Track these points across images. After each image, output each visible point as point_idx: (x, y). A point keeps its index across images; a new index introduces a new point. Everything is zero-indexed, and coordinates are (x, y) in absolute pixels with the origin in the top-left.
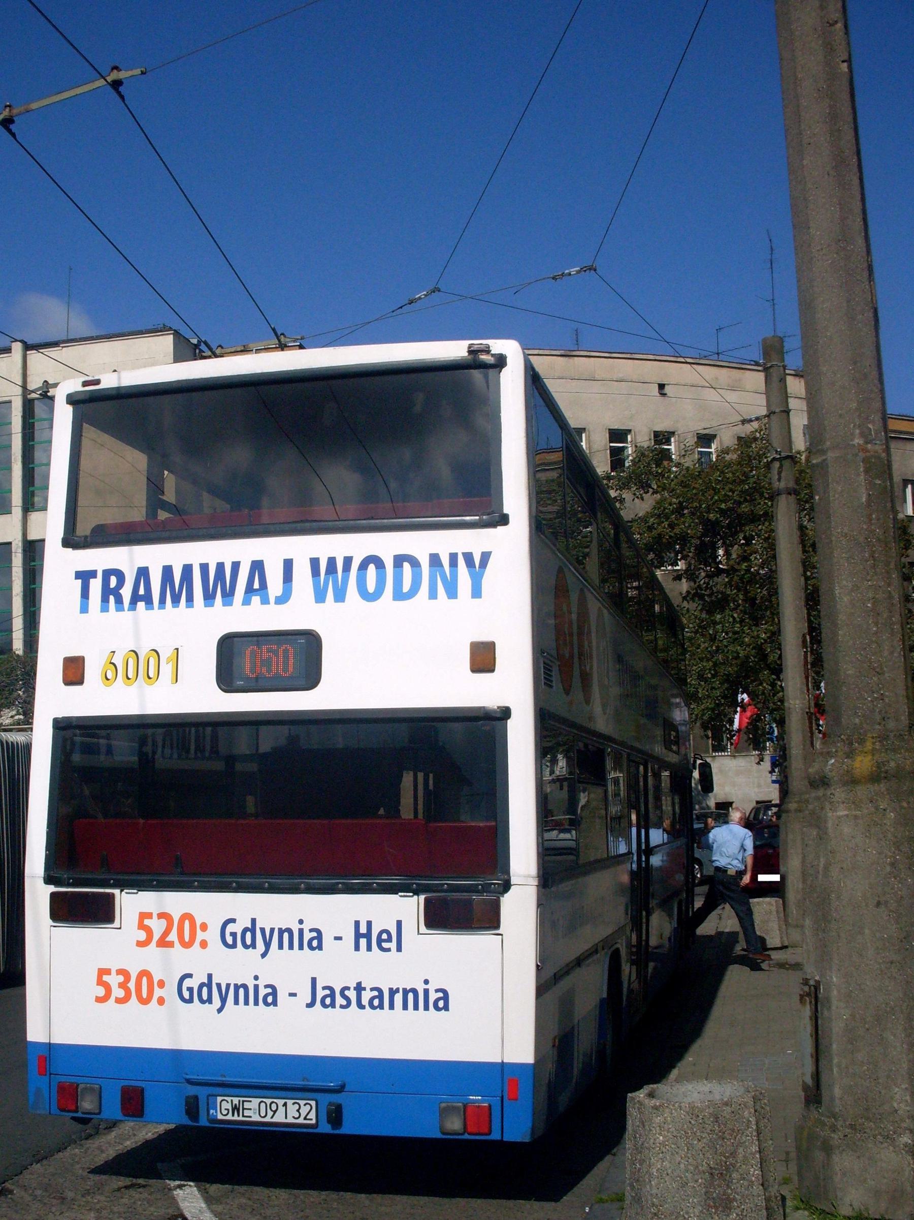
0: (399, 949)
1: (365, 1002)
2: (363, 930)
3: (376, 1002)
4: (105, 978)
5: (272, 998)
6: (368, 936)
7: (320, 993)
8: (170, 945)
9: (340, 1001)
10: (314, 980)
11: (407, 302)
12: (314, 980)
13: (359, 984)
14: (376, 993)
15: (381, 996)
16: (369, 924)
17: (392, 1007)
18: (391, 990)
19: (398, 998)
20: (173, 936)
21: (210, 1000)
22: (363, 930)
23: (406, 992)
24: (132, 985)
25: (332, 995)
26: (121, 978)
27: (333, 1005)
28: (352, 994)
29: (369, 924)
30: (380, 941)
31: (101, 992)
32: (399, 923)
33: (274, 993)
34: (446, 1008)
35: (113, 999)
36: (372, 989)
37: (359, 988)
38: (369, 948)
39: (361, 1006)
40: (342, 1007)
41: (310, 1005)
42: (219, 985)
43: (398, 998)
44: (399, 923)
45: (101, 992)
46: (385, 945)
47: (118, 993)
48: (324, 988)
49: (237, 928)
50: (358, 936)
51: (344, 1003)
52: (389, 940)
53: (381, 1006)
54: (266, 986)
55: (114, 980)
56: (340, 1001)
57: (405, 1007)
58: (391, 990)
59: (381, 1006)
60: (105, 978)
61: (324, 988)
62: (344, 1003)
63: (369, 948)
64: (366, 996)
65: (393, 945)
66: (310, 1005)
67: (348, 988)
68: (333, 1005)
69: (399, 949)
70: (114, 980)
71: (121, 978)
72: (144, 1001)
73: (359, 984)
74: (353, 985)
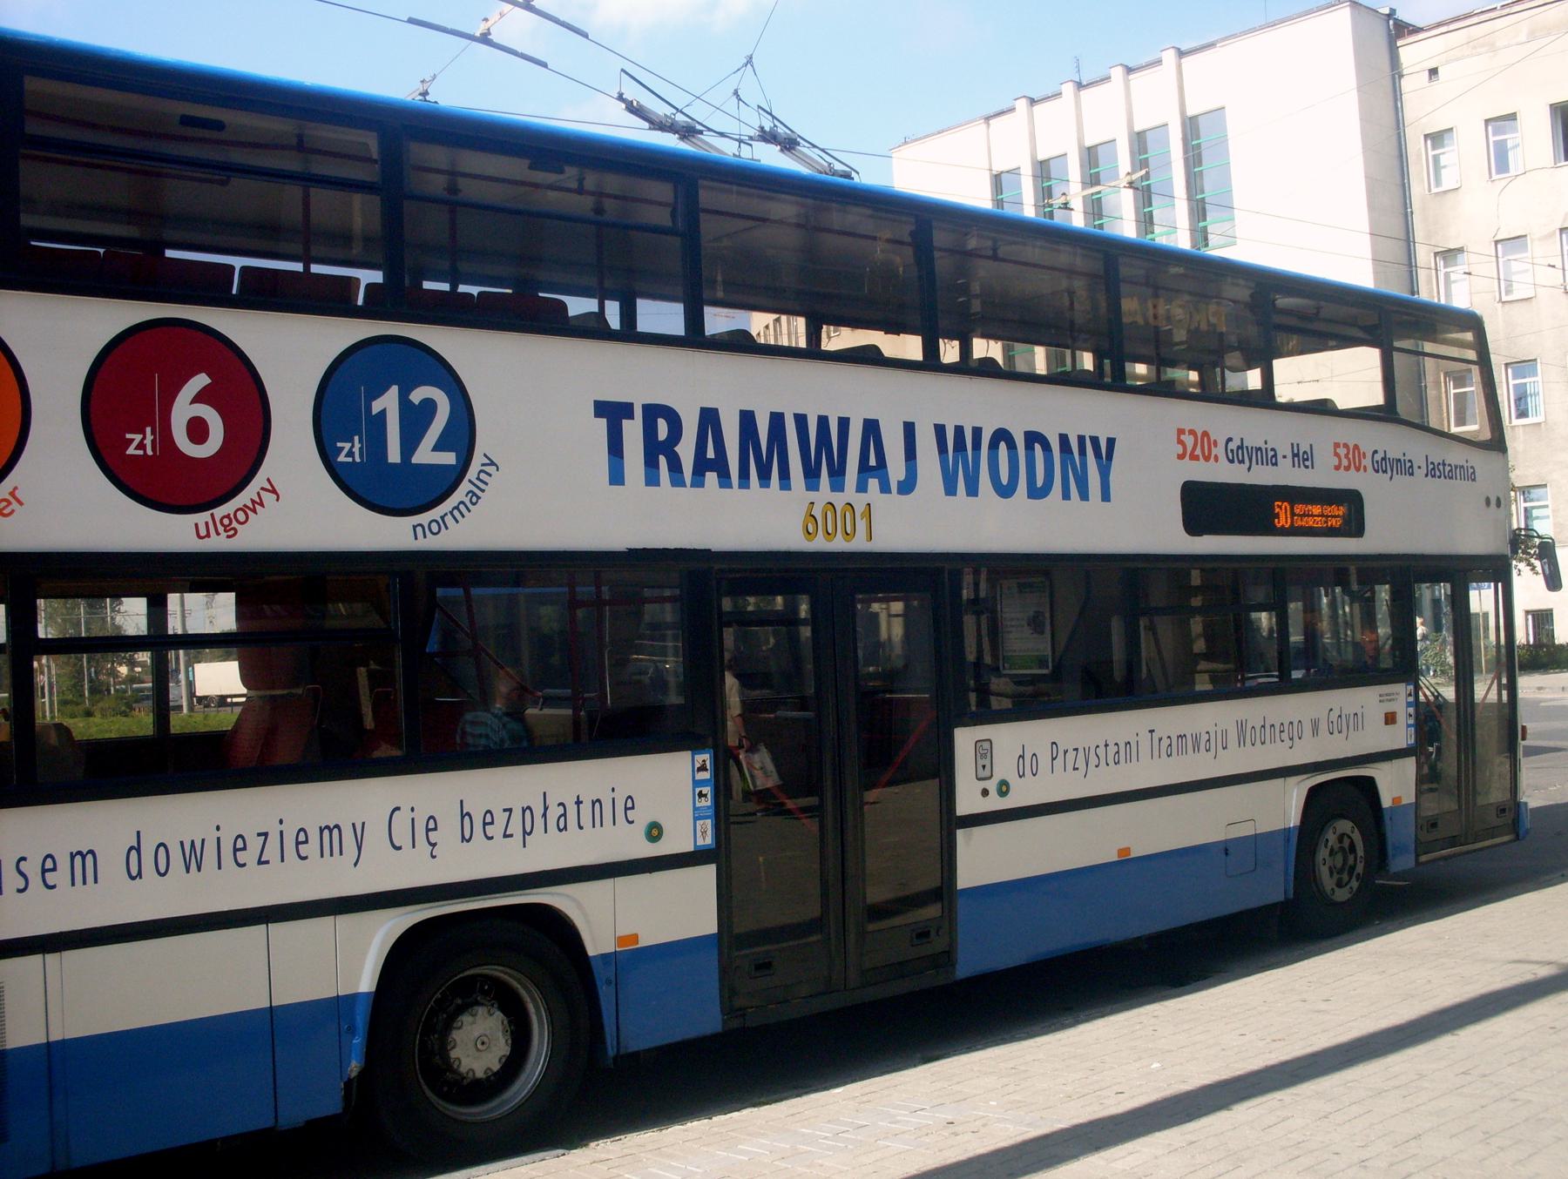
6: (1297, 455)
20: (1198, 452)
47: (1345, 462)
49: (1378, 457)
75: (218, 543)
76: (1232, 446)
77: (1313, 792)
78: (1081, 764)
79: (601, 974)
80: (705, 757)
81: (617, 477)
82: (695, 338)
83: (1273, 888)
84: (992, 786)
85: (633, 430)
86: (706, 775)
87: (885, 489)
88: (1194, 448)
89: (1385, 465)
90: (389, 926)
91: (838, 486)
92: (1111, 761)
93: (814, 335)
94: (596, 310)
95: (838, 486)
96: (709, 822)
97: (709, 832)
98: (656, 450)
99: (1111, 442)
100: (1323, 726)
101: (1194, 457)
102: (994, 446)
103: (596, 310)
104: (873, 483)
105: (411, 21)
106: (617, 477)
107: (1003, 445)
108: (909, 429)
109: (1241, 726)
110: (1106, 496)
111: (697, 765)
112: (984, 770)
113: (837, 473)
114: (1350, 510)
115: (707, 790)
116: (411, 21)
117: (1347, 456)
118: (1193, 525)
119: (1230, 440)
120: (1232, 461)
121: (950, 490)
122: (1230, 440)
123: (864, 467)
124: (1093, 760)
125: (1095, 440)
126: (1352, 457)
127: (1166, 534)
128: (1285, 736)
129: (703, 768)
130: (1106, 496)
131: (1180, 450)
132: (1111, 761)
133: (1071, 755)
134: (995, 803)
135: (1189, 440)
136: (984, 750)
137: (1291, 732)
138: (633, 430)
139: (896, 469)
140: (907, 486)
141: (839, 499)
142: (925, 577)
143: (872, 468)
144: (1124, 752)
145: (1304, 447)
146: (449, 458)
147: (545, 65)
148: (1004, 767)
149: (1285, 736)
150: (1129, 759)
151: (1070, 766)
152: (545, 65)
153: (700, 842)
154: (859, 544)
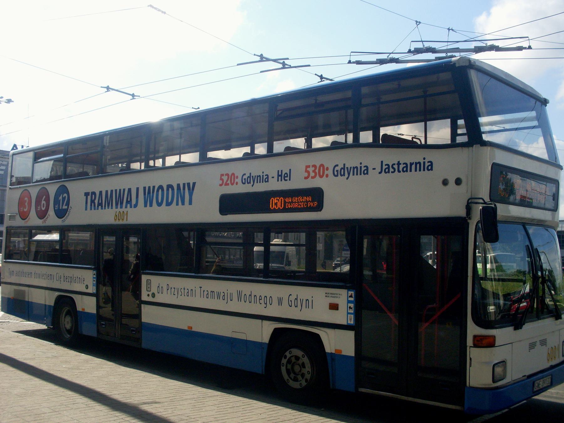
0: (290, 180)
1: (401, 169)
2: (280, 174)
3: (405, 169)
4: (308, 169)
5: (366, 171)
6: (281, 176)
7: (384, 167)
8: (228, 184)
9: (391, 170)
10: (382, 162)
11: (112, 92)
12: (382, 162)
13: (399, 162)
14: (405, 165)
15: (407, 167)
16: (282, 171)
17: (411, 171)
18: (410, 163)
19: (413, 166)
20: (229, 182)
21: (344, 175)
22: (280, 174)
23: (416, 164)
24: (317, 171)
25: (389, 168)
26: (313, 169)
27: (389, 172)
28: (396, 167)
29: (282, 171)
30: (285, 177)
31: (306, 175)
32: (290, 170)
33: (367, 169)
34: (432, 169)
35: (310, 177)
36: (404, 164)
37: (399, 164)
38: (281, 180)
39: (399, 171)
40: (392, 172)
41: (380, 173)
42: (347, 168)
43: (413, 166)
44: (290, 170)
45: (306, 175)
46: (286, 178)
47: (312, 174)
48: (386, 165)
49: (245, 177)
50: (279, 176)
51: (393, 170)
52: (287, 177)
53: (407, 171)
54: (364, 167)
55: (311, 169)
56: (391, 170)
57: (416, 171)
58: (410, 163)
59: (407, 171)
60: (308, 169)
61: (386, 165)
62: (393, 170)
63: (281, 180)
64: (401, 167)
65: (288, 178)
66: (380, 173)
67: (394, 164)
68: (389, 172)
69: (290, 180)
70: (311, 169)
71: (313, 169)
72: (321, 177)
73: (399, 162)
74: (396, 163)
75: (44, 224)
76: (337, 168)
77: (276, 331)
78: (176, 293)
79: (329, 359)
80: (352, 293)
81: (86, 209)
82: (149, 169)
83: (257, 366)
84: (150, 293)
85: (89, 197)
86: (352, 299)
87: (131, 207)
88: (227, 181)
89: (343, 172)
90: (57, 294)
91: (121, 207)
92: (186, 294)
93: (309, 143)
94: (314, 140)
95: (121, 207)
96: (352, 316)
97: (353, 319)
98: (93, 202)
99: (194, 184)
100: (285, 302)
101: (227, 184)
102: (158, 191)
103: (314, 140)
104: (129, 205)
105: (261, 72)
106: (86, 209)
107: (160, 190)
108: (138, 189)
109: (239, 294)
110: (190, 203)
111: (349, 295)
112: (149, 289)
113: (122, 203)
114: (316, 197)
115: (352, 305)
116: (261, 72)
117: (314, 171)
118: (223, 210)
119: (245, 174)
120: (244, 183)
121: (146, 206)
122: (245, 174)
123: (127, 202)
124: (180, 293)
125: (189, 184)
126: (321, 171)
127: (213, 215)
128: (262, 301)
129: (351, 296)
130: (190, 203)
131: (221, 182)
132: (186, 294)
133: (173, 290)
134: (150, 299)
135: (225, 178)
136: (149, 282)
137: (267, 301)
138: (89, 197)
139: (134, 202)
140: (136, 206)
141: (121, 210)
142: (144, 231)
143: (129, 202)
144: (190, 293)
145: (286, 171)
146: (66, 207)
147: (309, 66)
148: (154, 289)
149: (262, 301)
150: (192, 295)
151: (172, 294)
152: (309, 66)
153: (349, 322)
154: (125, 222)
